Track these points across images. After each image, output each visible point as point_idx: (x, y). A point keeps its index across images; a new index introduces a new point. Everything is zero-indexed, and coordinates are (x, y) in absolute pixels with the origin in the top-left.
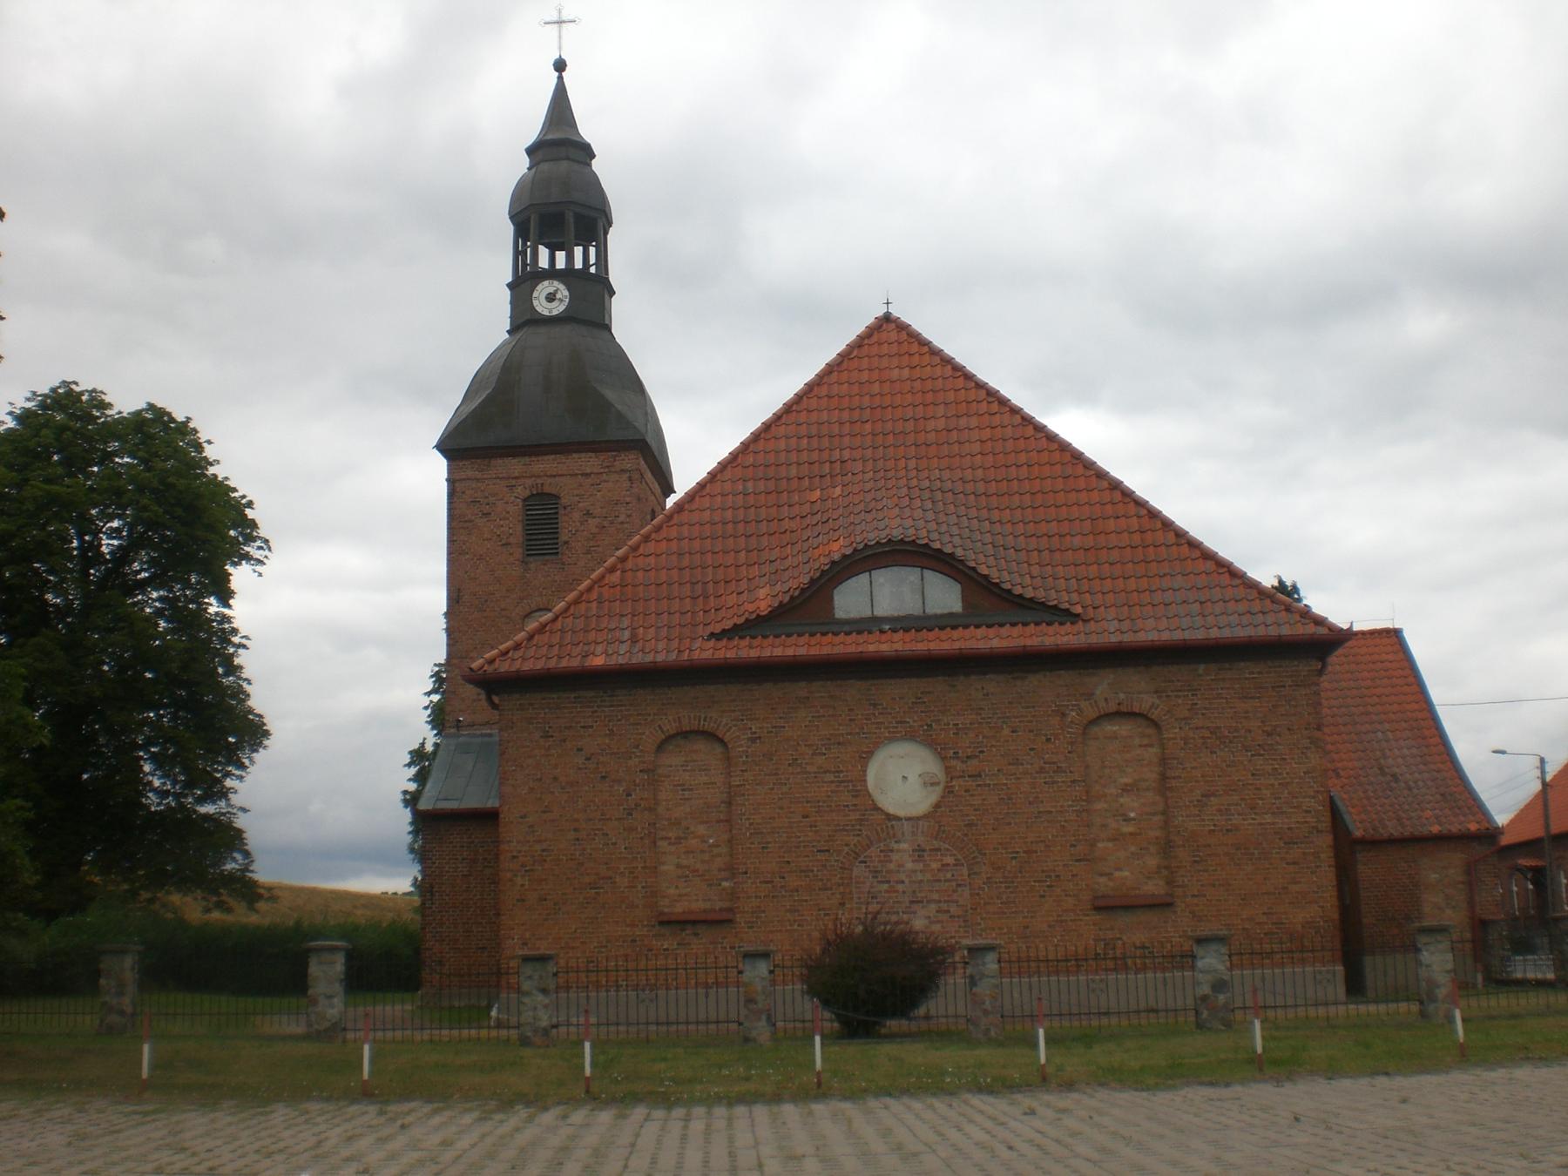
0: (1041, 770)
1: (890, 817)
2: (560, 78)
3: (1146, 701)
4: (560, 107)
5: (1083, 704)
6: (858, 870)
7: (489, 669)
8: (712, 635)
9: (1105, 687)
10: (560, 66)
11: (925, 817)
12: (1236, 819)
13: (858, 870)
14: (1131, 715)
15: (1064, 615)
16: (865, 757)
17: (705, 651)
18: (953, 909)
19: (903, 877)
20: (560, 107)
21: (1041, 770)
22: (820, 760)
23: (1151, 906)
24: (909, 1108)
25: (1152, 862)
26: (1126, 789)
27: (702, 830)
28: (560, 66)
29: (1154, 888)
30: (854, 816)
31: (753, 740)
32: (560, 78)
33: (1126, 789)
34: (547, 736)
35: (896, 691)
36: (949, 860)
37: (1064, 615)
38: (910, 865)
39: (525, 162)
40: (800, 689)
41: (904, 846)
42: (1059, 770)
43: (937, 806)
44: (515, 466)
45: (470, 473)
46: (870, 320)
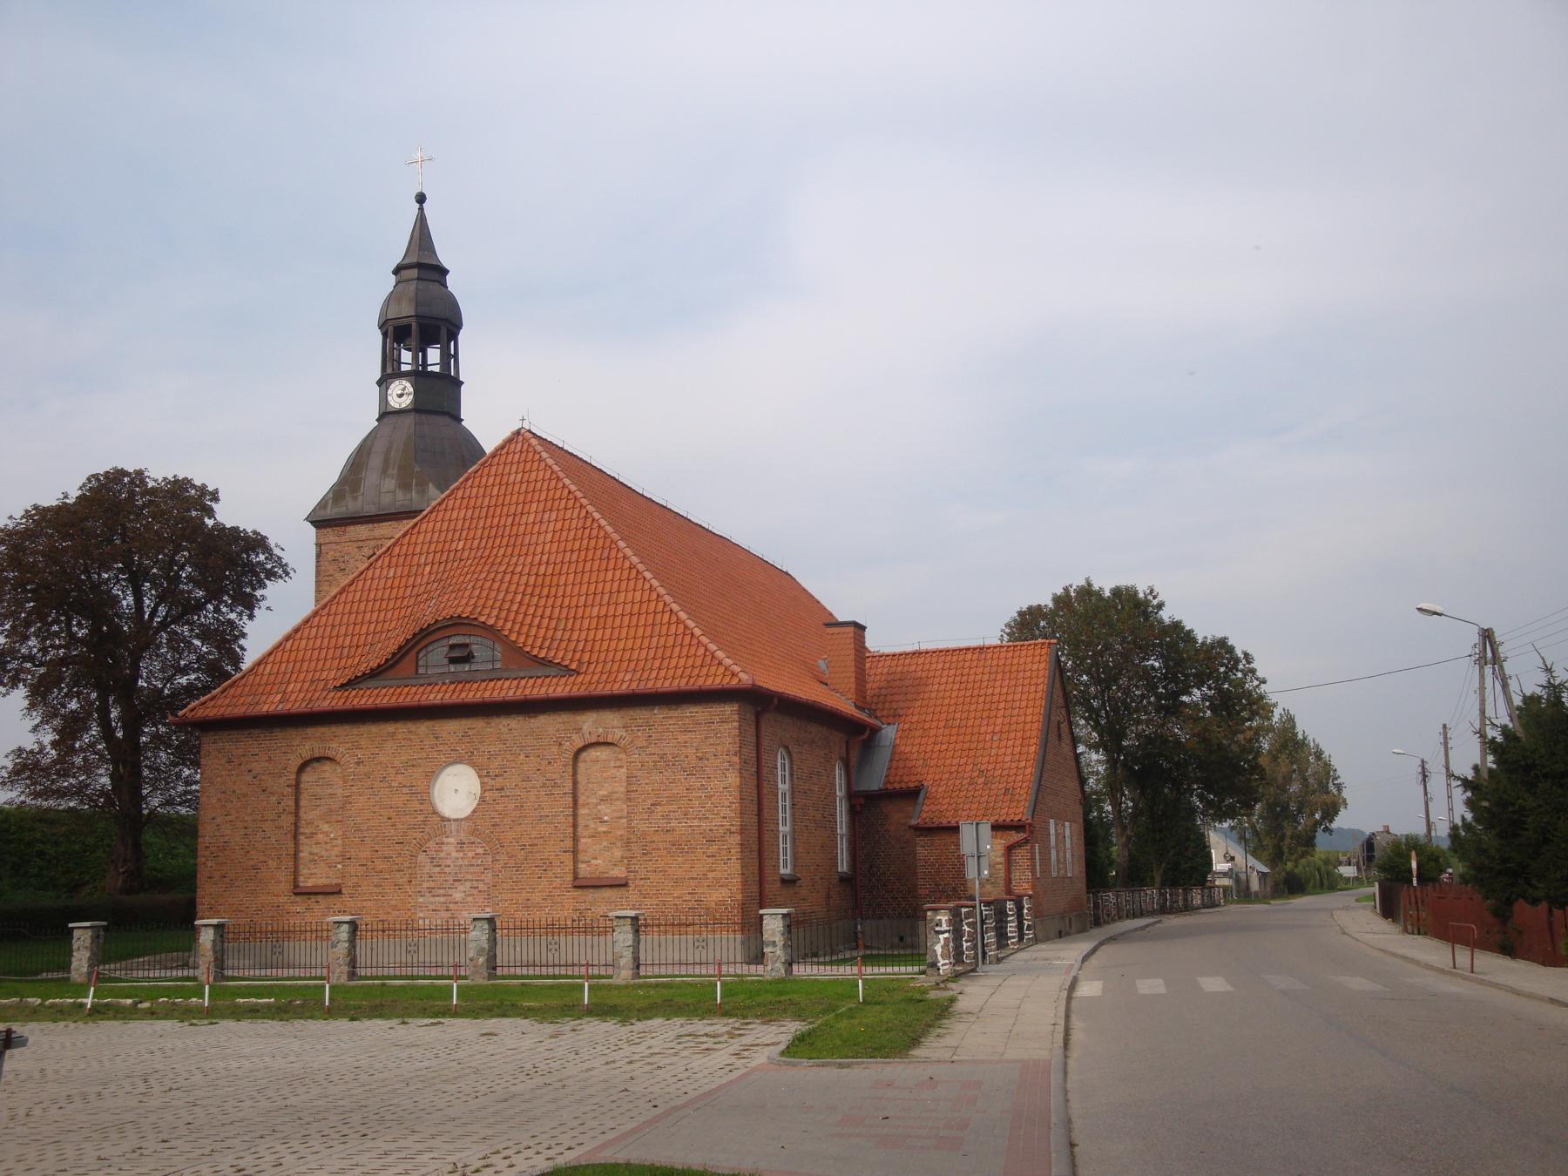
0: (544, 786)
1: (444, 819)
2: (421, 209)
3: (617, 734)
4: (421, 235)
5: (574, 737)
6: (422, 857)
7: (190, 715)
8: (342, 685)
9: (591, 724)
10: (421, 199)
11: (467, 819)
12: (674, 823)
13: (422, 857)
14: (598, 744)
15: (567, 671)
16: (431, 776)
17: (330, 702)
18: (482, 886)
19: (449, 862)
20: (421, 235)
21: (544, 786)
22: (400, 778)
23: (611, 886)
24: (926, 1061)
25: (618, 853)
26: (603, 800)
27: (326, 827)
28: (421, 199)
29: (618, 872)
30: (421, 818)
31: (358, 763)
32: (421, 209)
33: (603, 800)
34: (230, 762)
35: (451, 728)
36: (480, 851)
37: (567, 671)
38: (454, 854)
39: (393, 279)
40: (390, 728)
41: (451, 840)
42: (555, 785)
43: (474, 811)
44: (362, 531)
45: (333, 539)
46: (507, 434)
